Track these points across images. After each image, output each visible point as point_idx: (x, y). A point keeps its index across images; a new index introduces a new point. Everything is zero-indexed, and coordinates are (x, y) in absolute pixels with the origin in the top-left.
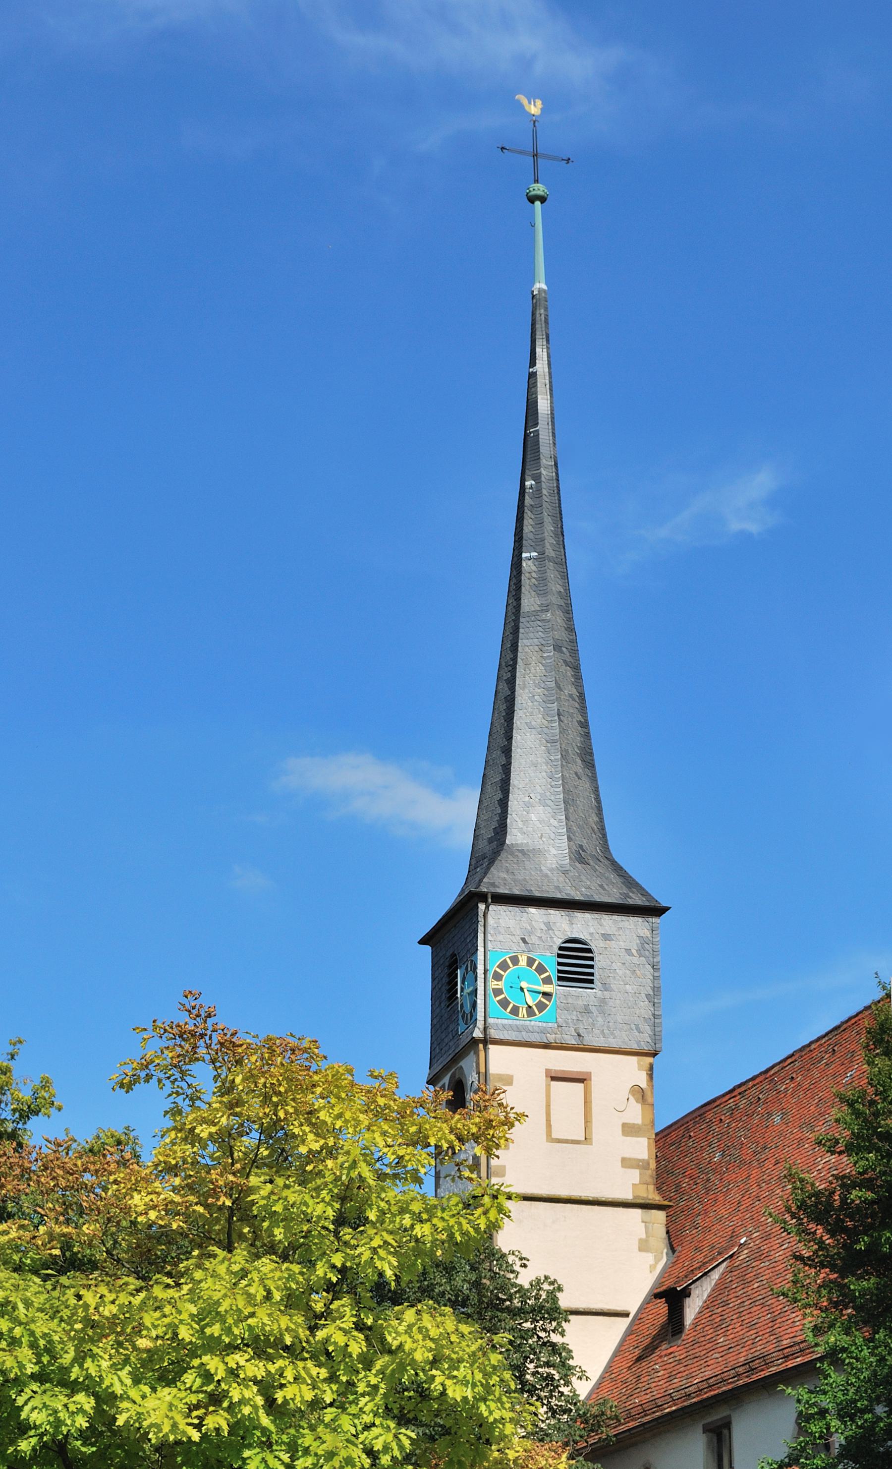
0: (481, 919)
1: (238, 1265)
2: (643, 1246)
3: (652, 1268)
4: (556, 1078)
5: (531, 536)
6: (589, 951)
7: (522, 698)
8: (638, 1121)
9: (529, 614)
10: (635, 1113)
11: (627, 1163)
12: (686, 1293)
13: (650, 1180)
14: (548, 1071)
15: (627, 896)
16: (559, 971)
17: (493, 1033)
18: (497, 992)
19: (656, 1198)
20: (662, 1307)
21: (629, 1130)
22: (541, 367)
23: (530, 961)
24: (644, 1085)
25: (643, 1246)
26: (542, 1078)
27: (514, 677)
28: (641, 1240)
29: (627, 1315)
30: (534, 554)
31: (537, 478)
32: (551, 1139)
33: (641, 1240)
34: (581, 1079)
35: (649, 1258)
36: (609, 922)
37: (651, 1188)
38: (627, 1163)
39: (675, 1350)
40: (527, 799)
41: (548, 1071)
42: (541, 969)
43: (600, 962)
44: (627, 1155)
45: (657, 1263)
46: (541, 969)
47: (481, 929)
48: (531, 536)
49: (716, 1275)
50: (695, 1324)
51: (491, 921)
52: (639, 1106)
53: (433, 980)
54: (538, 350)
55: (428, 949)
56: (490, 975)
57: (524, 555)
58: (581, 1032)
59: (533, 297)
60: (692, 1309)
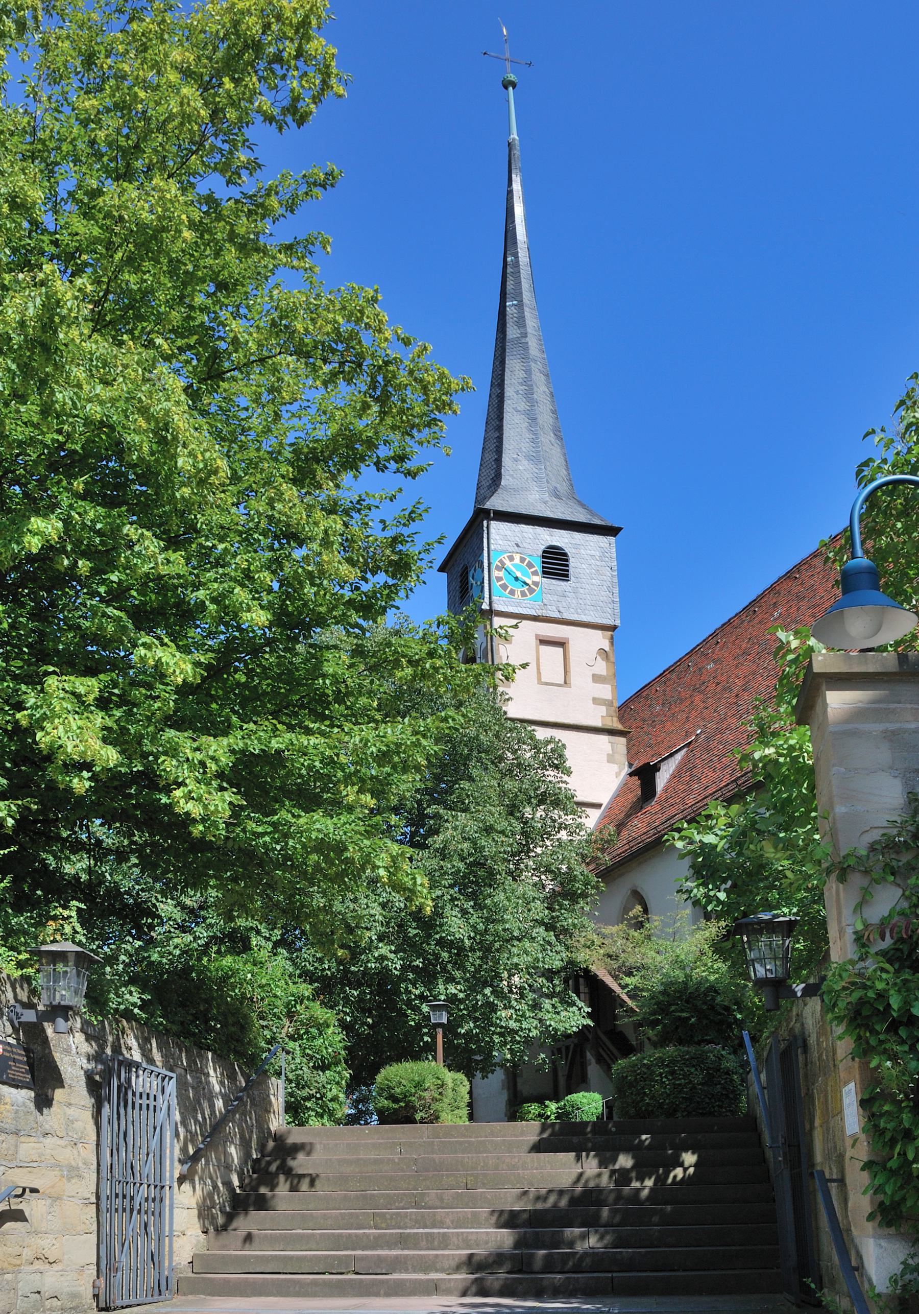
0: (485, 529)
1: (65, 196)
2: (611, 759)
3: (618, 775)
4: (544, 642)
5: (512, 291)
6: (565, 554)
7: (509, 391)
8: (604, 673)
9: (512, 340)
10: (601, 667)
11: (596, 701)
12: (656, 768)
13: (614, 714)
14: (537, 636)
15: (591, 520)
16: (543, 567)
17: (497, 607)
18: (499, 579)
19: (619, 726)
20: (636, 781)
21: (597, 679)
22: (517, 187)
23: (522, 560)
24: (607, 649)
25: (611, 759)
26: (533, 642)
27: (503, 381)
28: (608, 755)
29: (598, 806)
30: (515, 302)
31: (516, 255)
32: (540, 682)
33: (608, 755)
34: (561, 644)
35: (615, 768)
36: (578, 537)
37: (615, 719)
38: (596, 701)
39: (653, 806)
40: (515, 456)
41: (537, 636)
42: (530, 565)
43: (572, 563)
44: (596, 696)
45: (620, 771)
46: (530, 565)
47: (485, 535)
48: (512, 291)
49: (679, 757)
50: (666, 790)
51: (492, 530)
52: (604, 663)
53: (449, 593)
54: (514, 176)
55: (444, 575)
56: (493, 567)
57: (508, 304)
58: (561, 609)
59: (509, 144)
60: (662, 779)
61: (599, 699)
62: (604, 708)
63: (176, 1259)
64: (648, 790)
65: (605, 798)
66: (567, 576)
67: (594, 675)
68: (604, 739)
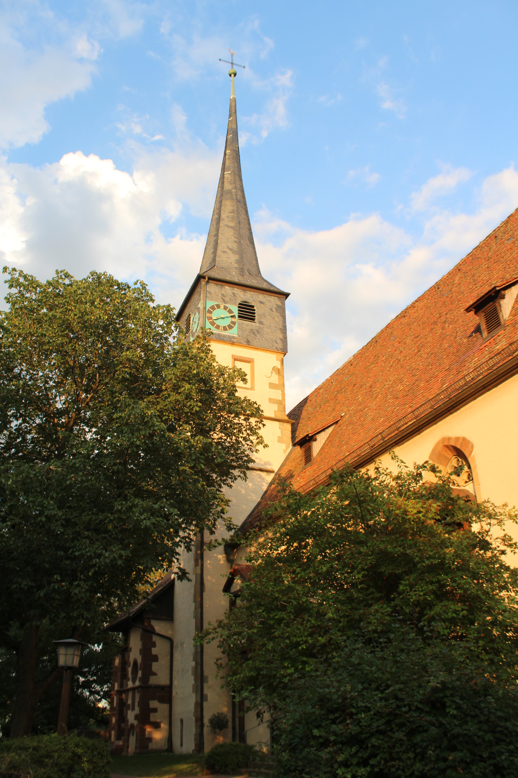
3: (285, 451)
14: (233, 356)
16: (239, 313)
28: (279, 437)
29: (273, 472)
33: (279, 437)
35: (284, 446)
41: (233, 356)
44: (271, 397)
61: (273, 399)
62: (276, 405)
63: (504, 317)
64: (308, 457)
65: (276, 468)
66: (254, 320)
67: (270, 384)
68: (277, 423)
